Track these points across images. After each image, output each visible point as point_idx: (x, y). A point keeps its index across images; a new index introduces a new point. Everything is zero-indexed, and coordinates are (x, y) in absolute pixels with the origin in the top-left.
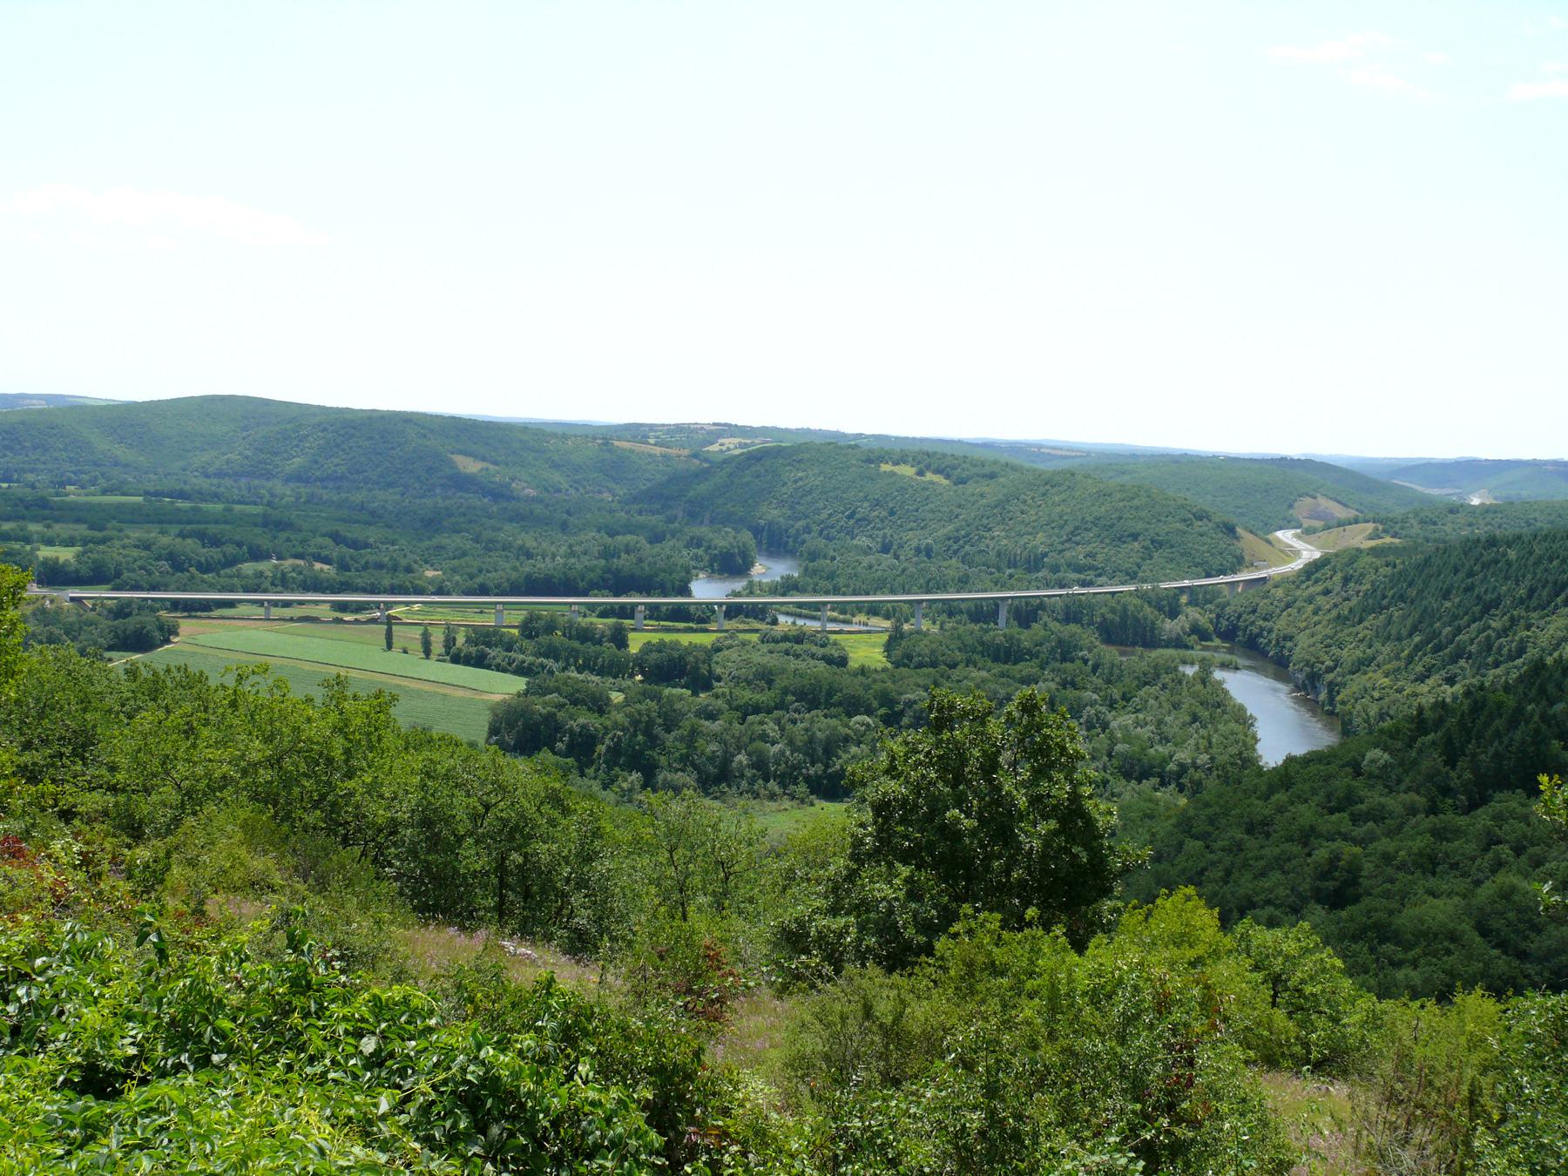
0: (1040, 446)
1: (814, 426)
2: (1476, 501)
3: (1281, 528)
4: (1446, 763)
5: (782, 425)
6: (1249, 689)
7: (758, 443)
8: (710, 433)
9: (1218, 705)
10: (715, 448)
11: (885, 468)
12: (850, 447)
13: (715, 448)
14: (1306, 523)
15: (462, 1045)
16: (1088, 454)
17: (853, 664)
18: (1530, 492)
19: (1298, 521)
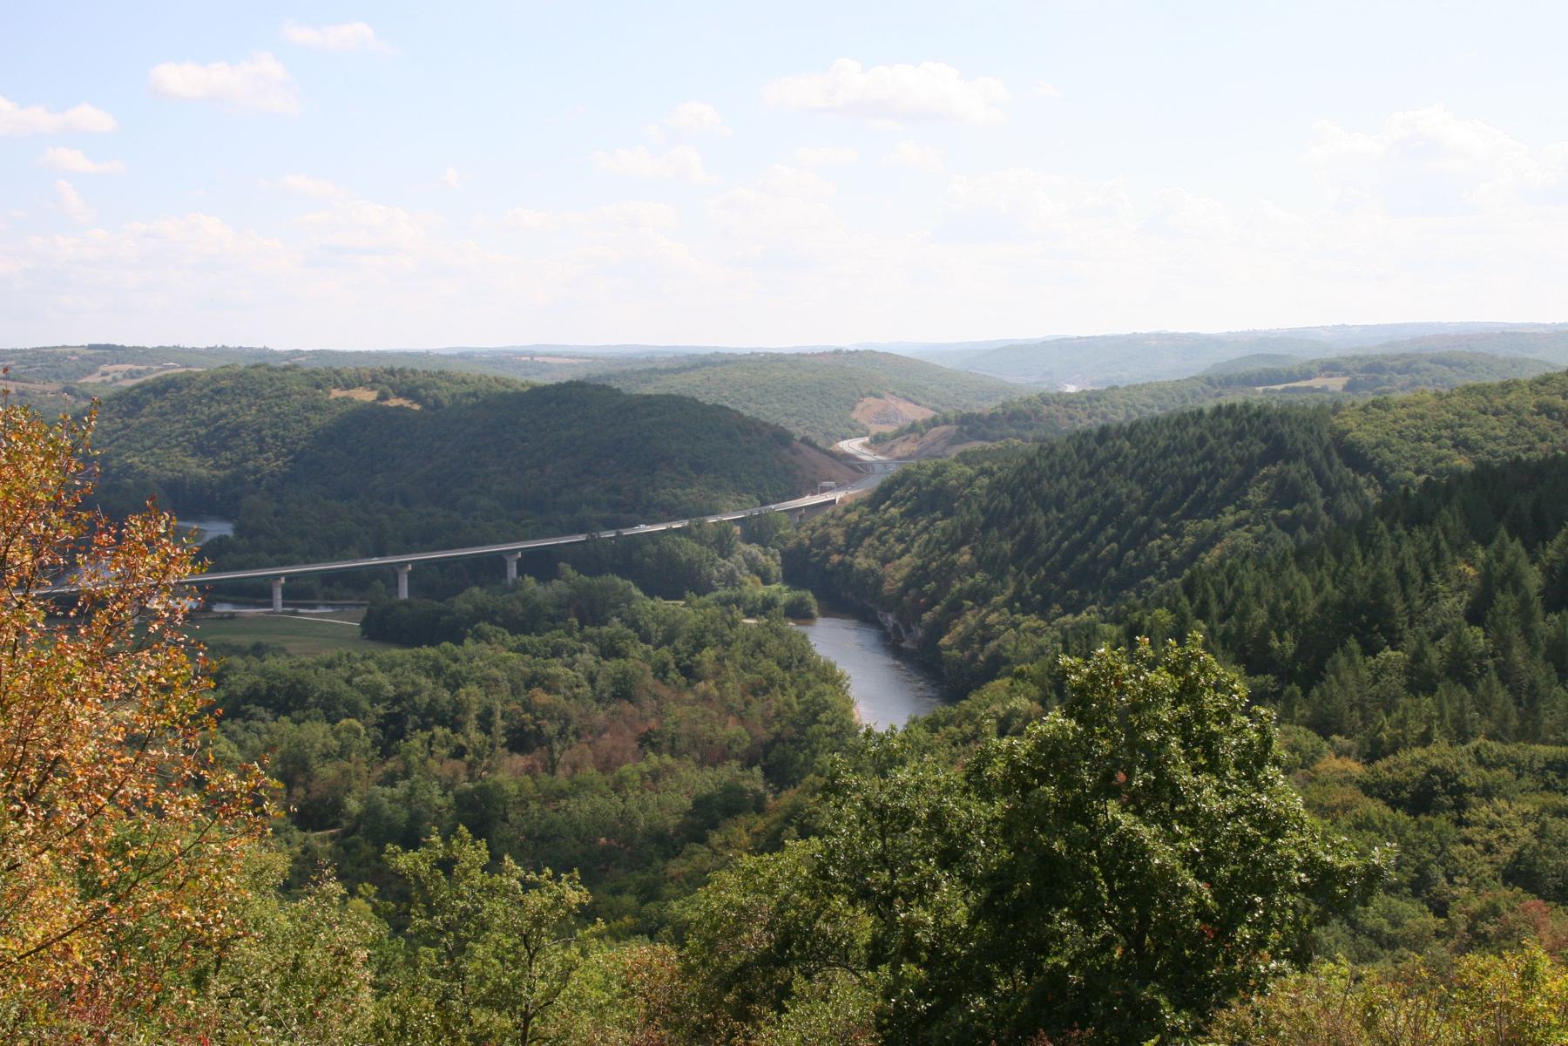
0: (533, 355)
1: (232, 343)
2: (1071, 389)
3: (844, 438)
4: (1516, 731)
5: (187, 344)
6: (835, 644)
7: (154, 374)
8: (84, 358)
9: (798, 661)
10: (94, 379)
11: (336, 393)
12: (286, 369)
13: (94, 379)
14: (875, 429)
15: (61, 922)
16: (595, 359)
17: (1207, 411)
18: (1131, 374)
19: (862, 427)
